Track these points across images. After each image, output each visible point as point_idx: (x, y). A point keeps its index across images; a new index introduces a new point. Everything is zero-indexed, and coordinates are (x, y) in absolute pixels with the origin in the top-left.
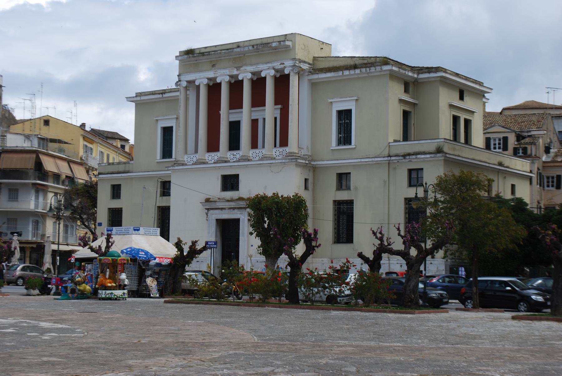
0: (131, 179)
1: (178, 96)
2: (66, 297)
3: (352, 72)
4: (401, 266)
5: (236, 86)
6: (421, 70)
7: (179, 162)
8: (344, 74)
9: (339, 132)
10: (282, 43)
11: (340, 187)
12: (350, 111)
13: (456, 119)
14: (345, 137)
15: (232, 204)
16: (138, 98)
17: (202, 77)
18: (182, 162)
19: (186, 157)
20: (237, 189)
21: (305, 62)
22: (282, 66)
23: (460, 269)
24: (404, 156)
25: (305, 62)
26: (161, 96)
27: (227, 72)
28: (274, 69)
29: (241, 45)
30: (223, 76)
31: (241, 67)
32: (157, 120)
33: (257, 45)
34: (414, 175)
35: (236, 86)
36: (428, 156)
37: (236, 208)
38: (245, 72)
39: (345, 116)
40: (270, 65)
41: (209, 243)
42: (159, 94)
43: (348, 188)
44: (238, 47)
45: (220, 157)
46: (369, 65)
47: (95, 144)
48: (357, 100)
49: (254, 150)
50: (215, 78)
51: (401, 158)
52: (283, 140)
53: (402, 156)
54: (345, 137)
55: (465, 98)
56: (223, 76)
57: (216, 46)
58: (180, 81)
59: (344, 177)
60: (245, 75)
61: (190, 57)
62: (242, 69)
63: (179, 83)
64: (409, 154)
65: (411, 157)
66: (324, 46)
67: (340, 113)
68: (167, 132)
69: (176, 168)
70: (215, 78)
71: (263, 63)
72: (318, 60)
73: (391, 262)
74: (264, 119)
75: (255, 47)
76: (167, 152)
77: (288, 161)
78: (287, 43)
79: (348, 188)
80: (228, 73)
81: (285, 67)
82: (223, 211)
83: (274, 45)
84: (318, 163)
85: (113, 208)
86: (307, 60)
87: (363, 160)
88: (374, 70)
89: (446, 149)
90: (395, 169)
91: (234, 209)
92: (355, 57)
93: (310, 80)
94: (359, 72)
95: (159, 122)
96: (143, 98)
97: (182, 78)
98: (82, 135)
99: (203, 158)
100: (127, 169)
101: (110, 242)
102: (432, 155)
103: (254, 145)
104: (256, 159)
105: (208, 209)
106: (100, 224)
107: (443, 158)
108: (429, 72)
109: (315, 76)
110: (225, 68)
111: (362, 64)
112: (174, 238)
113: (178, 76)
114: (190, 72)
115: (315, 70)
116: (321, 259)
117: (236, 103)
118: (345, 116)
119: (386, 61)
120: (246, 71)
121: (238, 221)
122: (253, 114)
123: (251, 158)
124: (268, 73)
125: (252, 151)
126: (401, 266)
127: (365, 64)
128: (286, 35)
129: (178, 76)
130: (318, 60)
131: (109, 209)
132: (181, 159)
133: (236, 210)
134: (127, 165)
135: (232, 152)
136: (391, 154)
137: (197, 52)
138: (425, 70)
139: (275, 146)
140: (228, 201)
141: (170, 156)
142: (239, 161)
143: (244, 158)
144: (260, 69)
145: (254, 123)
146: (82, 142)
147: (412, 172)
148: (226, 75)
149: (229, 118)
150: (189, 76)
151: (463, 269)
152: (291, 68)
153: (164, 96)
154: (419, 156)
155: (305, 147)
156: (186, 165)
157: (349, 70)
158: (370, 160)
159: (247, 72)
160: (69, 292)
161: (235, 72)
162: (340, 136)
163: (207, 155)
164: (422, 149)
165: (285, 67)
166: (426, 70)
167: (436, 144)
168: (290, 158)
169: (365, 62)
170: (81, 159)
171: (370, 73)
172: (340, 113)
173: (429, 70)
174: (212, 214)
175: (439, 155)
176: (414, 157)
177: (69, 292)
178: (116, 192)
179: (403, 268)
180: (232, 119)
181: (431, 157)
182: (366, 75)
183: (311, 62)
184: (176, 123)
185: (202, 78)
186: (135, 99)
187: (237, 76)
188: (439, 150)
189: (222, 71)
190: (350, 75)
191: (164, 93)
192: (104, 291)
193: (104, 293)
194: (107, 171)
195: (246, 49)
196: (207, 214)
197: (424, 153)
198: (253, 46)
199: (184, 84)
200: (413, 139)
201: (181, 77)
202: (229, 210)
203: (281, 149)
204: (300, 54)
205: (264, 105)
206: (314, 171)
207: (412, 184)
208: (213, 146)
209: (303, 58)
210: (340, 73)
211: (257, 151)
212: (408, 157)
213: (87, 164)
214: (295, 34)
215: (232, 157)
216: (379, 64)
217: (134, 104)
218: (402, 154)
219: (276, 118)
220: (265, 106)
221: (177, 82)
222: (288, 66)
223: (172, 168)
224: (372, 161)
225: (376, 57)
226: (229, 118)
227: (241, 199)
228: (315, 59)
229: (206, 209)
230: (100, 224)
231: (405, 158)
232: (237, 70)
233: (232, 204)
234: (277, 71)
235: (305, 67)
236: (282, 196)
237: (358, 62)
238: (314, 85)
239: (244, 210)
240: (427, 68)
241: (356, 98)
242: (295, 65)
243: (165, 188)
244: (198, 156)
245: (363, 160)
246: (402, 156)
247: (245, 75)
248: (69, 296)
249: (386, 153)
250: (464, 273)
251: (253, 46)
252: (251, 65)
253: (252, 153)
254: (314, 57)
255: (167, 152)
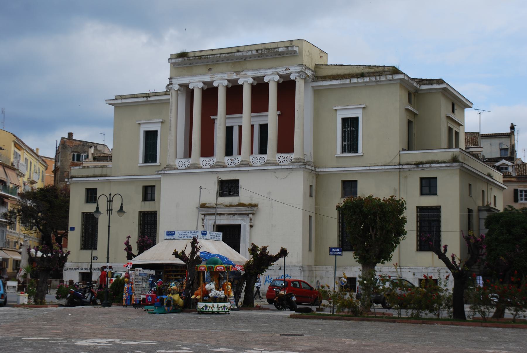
0: (109, 181)
1: (169, 99)
2: (162, 311)
3: (361, 80)
4: (414, 274)
5: (234, 91)
6: (421, 81)
7: (170, 166)
8: (352, 82)
9: (344, 139)
10: (290, 48)
11: (145, 198)
12: (156, 132)
13: (450, 129)
14: (350, 142)
15: (233, 210)
16: (119, 101)
17: (197, 80)
18: (174, 166)
19: (177, 161)
20: (237, 194)
21: (309, 69)
22: (287, 72)
23: (478, 278)
24: (417, 164)
25: (309, 69)
26: (145, 99)
27: (226, 76)
28: (278, 74)
29: (241, 49)
30: (221, 80)
31: (242, 71)
32: (139, 124)
33: (262, 50)
34: (149, 191)
35: (234, 91)
36: (443, 165)
37: (236, 214)
38: (245, 77)
39: (350, 125)
40: (274, 70)
41: (333, 250)
42: (143, 97)
43: (153, 199)
44: (238, 51)
45: (218, 162)
46: (377, 74)
47: (22, 151)
48: (162, 122)
49: (230, 157)
50: (212, 82)
51: (413, 166)
52: (286, 144)
53: (415, 164)
54: (350, 142)
55: (455, 111)
56: (221, 80)
57: (212, 50)
58: (171, 84)
59: (150, 189)
60: (246, 80)
61: (183, 60)
62: (242, 73)
63: (170, 86)
64: (422, 163)
65: (424, 166)
66: (322, 55)
67: (345, 121)
68: (151, 137)
69: (168, 172)
70: (212, 82)
71: (266, 69)
72: (320, 68)
73: (403, 270)
74: (240, 127)
75: (260, 52)
76: (150, 155)
77: (295, 167)
78: (296, 49)
79: (153, 199)
80: (226, 77)
81: (291, 73)
82: (222, 216)
83: (281, 50)
84: (322, 170)
85: (87, 213)
86: (310, 67)
87: (371, 168)
88: (384, 79)
89: (460, 159)
90: (406, 177)
91: (234, 214)
92: (361, 66)
93: (313, 87)
94: (368, 80)
95: (339, 113)
96: (125, 101)
97: (174, 81)
98: (14, 141)
99: (197, 162)
100: (104, 173)
101: (196, 247)
102: (448, 165)
103: (229, 152)
104: (256, 165)
105: (204, 215)
106: (73, 229)
107: (459, 168)
108: (432, 84)
109: (320, 83)
110: (222, 73)
111: (369, 73)
112: (245, 246)
113: (169, 79)
114: (183, 76)
115: (317, 78)
116: (325, 267)
117: (234, 106)
118: (350, 125)
119: (395, 71)
120: (246, 76)
121: (238, 227)
122: (227, 121)
123: (252, 163)
124: (272, 78)
125: (227, 158)
126: (414, 274)
127: (373, 73)
128: (292, 41)
129: (169, 79)
130: (320, 68)
131: (83, 213)
132: (172, 163)
133: (236, 217)
134: (105, 169)
135: (205, 158)
136: (401, 163)
137: (191, 55)
138: (426, 82)
139: (252, 153)
140: (227, 206)
141: (154, 160)
142: (239, 166)
143: (245, 163)
144: (262, 74)
145: (229, 130)
146: (13, 148)
147: (423, 181)
148: (224, 80)
149: (225, 123)
150: (180, 79)
151: (481, 278)
152: (297, 74)
153: (149, 99)
154: (433, 165)
155: (309, 155)
156: (177, 169)
157: (358, 78)
158: (380, 168)
159: (248, 77)
160: (165, 304)
161: (234, 77)
162: (344, 143)
163: (202, 159)
164: (436, 158)
165: (291, 73)
166: (427, 82)
167: (451, 154)
168: (297, 164)
169: (373, 70)
170: (12, 164)
171: (380, 81)
172: (345, 121)
173: (430, 82)
174: (209, 220)
175: (455, 164)
176: (428, 165)
177: (165, 304)
178: (91, 195)
179: (416, 276)
180: (228, 125)
181: (446, 166)
182: (374, 84)
183: (313, 69)
184: (161, 127)
185: (196, 81)
186: (116, 102)
187: (237, 80)
188: (455, 160)
189: (219, 76)
190: (358, 83)
191: (149, 97)
192: (215, 304)
193: (216, 307)
194: (81, 175)
195: (249, 53)
196: (203, 220)
197: (438, 162)
198: (257, 51)
199: (177, 87)
200: (454, 146)
201: (173, 80)
202: (229, 216)
203: (259, 156)
204: (306, 61)
205: (267, 110)
206: (317, 178)
207: (423, 193)
208: (207, 150)
209: (308, 65)
210: (348, 81)
211: (233, 158)
212: (421, 166)
213: (18, 170)
214: (302, 40)
215: (230, 162)
216: (388, 73)
217: (113, 107)
218: (413, 163)
219: (252, 126)
220: (217, 115)
221: (168, 85)
222: (295, 72)
223: (163, 172)
224: (382, 169)
225: (384, 66)
226: (225, 123)
227: (241, 205)
228: (317, 66)
229: (202, 214)
230: (73, 229)
231: (418, 167)
232: (237, 74)
233: (233, 210)
234: (281, 76)
235: (310, 73)
236: (384, 200)
237: (366, 70)
238: (317, 92)
239: (246, 216)
240: (427, 80)
241: (364, 106)
242: (301, 72)
243: (149, 193)
244: (191, 161)
245: (371, 168)
246: (415, 164)
247: (246, 80)
248: (165, 309)
249: (397, 161)
250: (481, 282)
251: (257, 51)
252: (253, 70)
253: (227, 160)
254: (316, 65)
255: (150, 155)
